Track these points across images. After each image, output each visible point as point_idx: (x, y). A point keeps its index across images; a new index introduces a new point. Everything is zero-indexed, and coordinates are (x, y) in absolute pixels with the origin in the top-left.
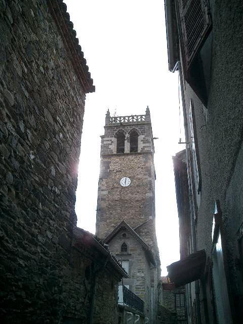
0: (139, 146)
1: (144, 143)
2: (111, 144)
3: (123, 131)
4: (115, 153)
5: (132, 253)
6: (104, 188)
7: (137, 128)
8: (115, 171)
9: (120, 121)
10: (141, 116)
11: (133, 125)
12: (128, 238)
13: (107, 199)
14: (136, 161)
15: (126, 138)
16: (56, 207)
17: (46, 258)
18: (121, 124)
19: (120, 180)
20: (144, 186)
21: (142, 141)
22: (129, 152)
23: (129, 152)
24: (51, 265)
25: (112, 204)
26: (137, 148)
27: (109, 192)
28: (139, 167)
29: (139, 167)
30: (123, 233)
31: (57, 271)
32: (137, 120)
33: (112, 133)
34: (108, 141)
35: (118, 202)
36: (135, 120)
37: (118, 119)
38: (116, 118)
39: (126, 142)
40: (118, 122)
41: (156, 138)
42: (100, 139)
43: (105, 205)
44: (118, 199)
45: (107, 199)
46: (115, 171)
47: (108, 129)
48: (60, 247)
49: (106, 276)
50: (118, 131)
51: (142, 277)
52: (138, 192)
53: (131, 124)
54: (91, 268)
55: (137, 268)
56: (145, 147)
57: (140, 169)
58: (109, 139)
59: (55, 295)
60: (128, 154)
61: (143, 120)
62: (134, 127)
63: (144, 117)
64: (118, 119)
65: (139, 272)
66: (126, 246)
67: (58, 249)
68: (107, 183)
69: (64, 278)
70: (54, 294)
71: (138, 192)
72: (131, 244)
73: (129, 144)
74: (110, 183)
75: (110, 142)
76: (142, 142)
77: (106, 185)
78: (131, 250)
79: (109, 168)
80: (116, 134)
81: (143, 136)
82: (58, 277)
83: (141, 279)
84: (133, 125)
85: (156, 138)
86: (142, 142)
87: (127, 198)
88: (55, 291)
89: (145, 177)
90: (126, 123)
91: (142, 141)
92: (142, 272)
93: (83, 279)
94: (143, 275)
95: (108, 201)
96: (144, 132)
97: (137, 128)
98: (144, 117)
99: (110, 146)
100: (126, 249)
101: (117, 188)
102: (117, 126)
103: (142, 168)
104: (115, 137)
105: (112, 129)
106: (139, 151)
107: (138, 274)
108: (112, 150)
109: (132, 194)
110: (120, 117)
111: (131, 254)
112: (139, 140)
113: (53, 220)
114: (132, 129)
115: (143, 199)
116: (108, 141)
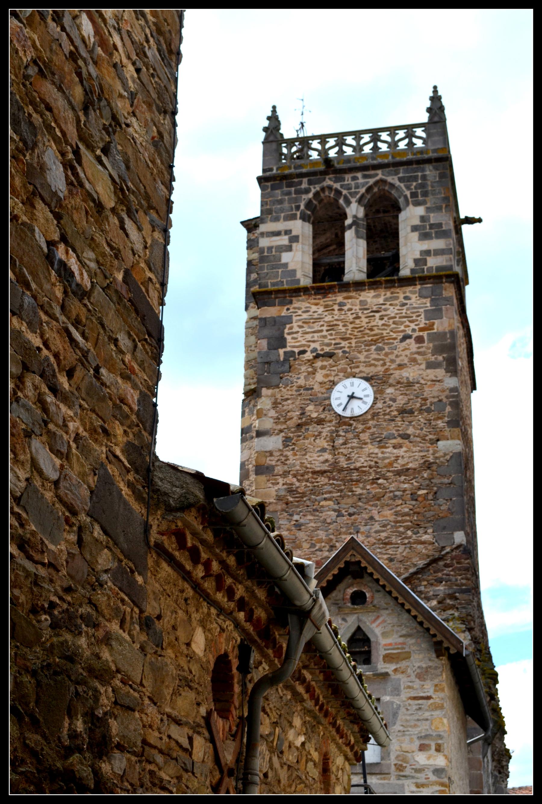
0: (403, 251)
1: (425, 236)
2: (289, 249)
3: (338, 193)
4: (306, 281)
5: (390, 668)
6: (268, 424)
7: (390, 179)
8: (309, 356)
9: (324, 152)
10: (410, 129)
11: (375, 167)
12: (377, 608)
13: (279, 469)
14: (392, 311)
15: (348, 222)
16: (72, 340)
17: (29, 565)
18: (328, 161)
19: (330, 389)
20: (429, 411)
21: (415, 228)
22: (362, 276)
23: (362, 276)
24: (53, 605)
25: (301, 486)
26: (396, 258)
27: (287, 441)
28: (408, 337)
29: (410, 337)
30: (350, 591)
31: (83, 641)
32: (393, 145)
33: (290, 201)
34: (277, 234)
35: (323, 480)
36: (384, 147)
37: (315, 144)
38: (305, 142)
39: (349, 235)
40: (314, 155)
41: (470, 221)
42: (244, 231)
43: (273, 491)
44: (325, 467)
45: (279, 469)
46: (309, 356)
47: (273, 188)
48: (97, 532)
49: (297, 722)
50: (316, 194)
51: (438, 771)
52: (406, 437)
53: (370, 162)
54: (235, 663)
55: (416, 731)
56: (427, 253)
57: (412, 344)
58: (280, 226)
59: (76, 757)
60: (358, 286)
61: (419, 143)
62: (380, 175)
63: (419, 132)
64: (315, 144)
65: (423, 748)
66: (366, 641)
67: (86, 537)
68: (275, 404)
69: (117, 682)
70: (68, 751)
71: (406, 437)
72: (385, 634)
73: (363, 244)
74: (288, 405)
75: (284, 240)
76: (416, 235)
77: (273, 413)
78: (388, 658)
79: (281, 342)
80: (309, 204)
81: (420, 211)
82: (90, 670)
83: (433, 778)
84: (375, 167)
85: (470, 221)
86: (416, 235)
87: (361, 461)
88: (74, 735)
89: (431, 374)
90: (349, 160)
91: (415, 228)
92: (438, 749)
93: (203, 711)
94: (440, 761)
95: (285, 474)
96: (425, 194)
97: (393, 179)
98: (419, 132)
99: (286, 257)
100: (368, 653)
101: (320, 422)
102: (314, 174)
103: (419, 340)
104: (304, 218)
105: (289, 185)
106: (405, 272)
107: (421, 759)
108: (294, 271)
109: (381, 443)
110: (323, 139)
111: (385, 675)
112: (401, 226)
113: (65, 398)
114: (371, 181)
115: (428, 465)
116: (277, 234)
